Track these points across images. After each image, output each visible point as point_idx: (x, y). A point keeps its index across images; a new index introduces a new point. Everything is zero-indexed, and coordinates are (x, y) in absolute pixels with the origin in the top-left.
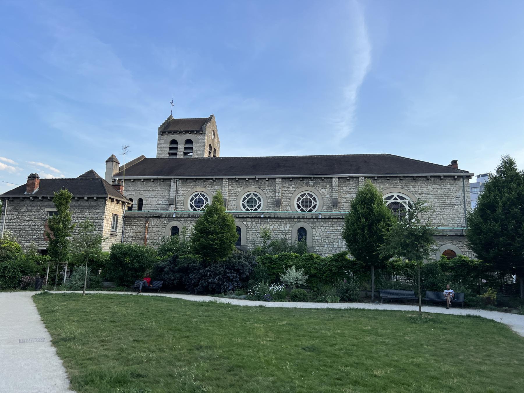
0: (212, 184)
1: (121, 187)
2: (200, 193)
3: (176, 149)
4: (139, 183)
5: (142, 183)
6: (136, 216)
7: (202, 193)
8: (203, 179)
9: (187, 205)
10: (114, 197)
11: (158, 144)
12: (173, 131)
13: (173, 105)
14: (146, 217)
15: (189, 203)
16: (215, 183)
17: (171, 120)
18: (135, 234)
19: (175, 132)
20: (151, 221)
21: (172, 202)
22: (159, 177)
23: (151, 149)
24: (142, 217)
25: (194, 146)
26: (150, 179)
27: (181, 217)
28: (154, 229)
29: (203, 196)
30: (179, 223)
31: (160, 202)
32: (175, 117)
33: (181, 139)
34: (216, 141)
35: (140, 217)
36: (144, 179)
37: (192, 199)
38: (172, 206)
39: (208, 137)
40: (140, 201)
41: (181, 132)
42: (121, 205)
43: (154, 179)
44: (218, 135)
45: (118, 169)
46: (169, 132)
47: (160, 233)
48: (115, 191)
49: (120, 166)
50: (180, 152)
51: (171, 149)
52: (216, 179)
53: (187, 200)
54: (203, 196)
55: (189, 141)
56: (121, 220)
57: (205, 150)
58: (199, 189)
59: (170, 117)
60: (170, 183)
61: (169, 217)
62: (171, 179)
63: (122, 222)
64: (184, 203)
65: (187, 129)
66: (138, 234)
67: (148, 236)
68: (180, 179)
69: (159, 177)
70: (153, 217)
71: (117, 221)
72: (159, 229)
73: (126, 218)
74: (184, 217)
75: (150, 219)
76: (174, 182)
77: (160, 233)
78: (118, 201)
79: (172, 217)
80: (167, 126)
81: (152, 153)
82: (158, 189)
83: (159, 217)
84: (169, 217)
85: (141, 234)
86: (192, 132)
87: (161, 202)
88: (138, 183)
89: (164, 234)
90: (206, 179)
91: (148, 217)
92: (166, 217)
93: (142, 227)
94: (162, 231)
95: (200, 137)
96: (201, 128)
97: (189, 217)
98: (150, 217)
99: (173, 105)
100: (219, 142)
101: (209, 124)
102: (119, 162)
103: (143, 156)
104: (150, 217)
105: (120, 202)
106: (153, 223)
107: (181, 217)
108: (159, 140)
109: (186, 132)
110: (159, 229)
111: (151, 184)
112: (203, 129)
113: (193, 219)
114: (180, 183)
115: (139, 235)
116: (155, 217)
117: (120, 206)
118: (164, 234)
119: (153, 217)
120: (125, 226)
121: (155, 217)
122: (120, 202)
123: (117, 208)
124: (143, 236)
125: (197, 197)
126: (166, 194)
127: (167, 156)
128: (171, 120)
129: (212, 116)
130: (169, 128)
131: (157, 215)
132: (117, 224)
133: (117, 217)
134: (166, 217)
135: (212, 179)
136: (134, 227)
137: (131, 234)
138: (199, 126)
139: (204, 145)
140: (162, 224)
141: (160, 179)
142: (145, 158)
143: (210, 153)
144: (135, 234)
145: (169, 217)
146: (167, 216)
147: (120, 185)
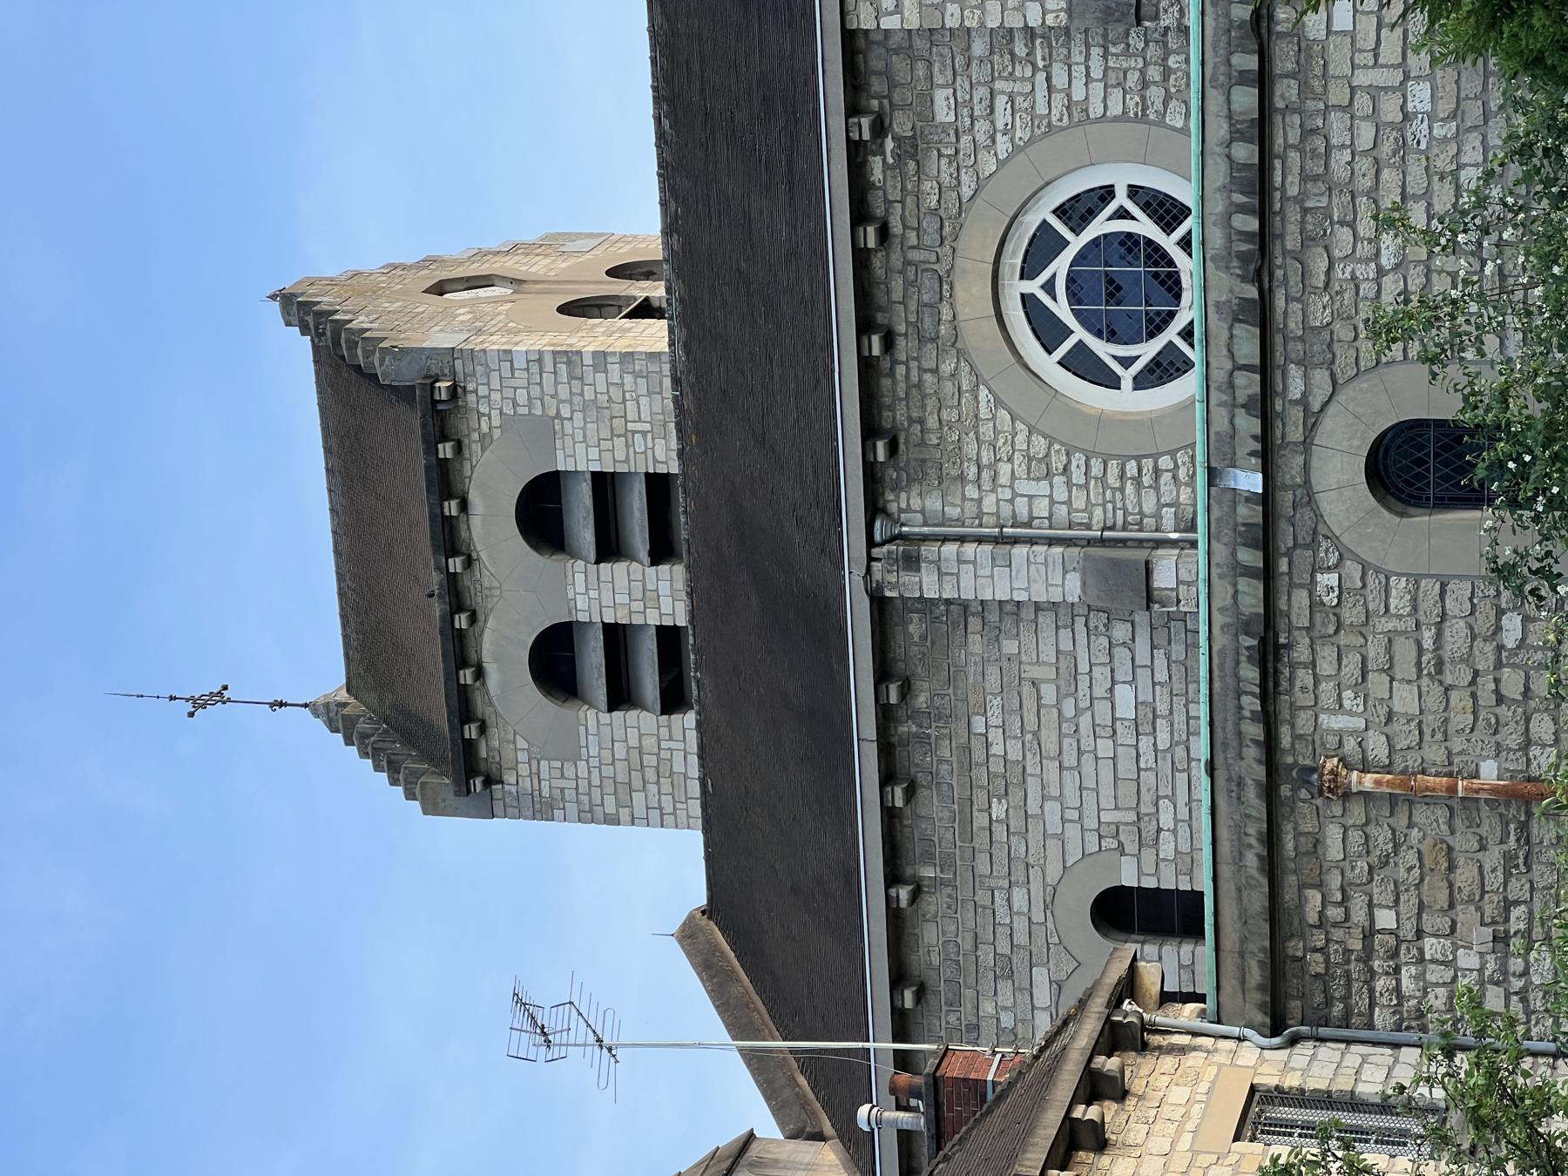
0: (912, 149)
1: (953, 1069)
2: (1015, 288)
3: (617, 637)
4: (930, 935)
5: (933, 903)
6: (1258, 900)
7: (1014, 259)
8: (861, 259)
9: (1152, 422)
10: (1051, 1121)
11: (587, 815)
12: (452, 677)
13: (220, 697)
14: (1270, 791)
15: (1127, 400)
16: (902, 124)
17: (355, 707)
18: (1466, 915)
19: (460, 651)
20: (1312, 741)
21: (1122, 578)
22: (864, 723)
23: (614, 876)
24: (1271, 839)
25: (581, 455)
26: (890, 816)
27: (1265, 406)
28: (1405, 700)
29: (1043, 247)
30: (1332, 423)
31: (1126, 709)
32: (327, 673)
33: (522, 596)
34: (537, 267)
35: (1272, 865)
36: (893, 878)
37: (1083, 365)
38: (1164, 578)
39: (504, 335)
40: (1119, 911)
41: (456, 596)
42: (1146, 1063)
43: (888, 777)
44: (482, 254)
45: (805, 1151)
46: (464, 707)
47: (1456, 634)
48: (995, 1121)
49: (767, 1127)
50: (650, 597)
51: (621, 696)
52: (853, 110)
53: (1102, 421)
54: (1043, 247)
55: (541, 512)
56: (1316, 1066)
57: (621, 345)
58: (971, 295)
59: (334, 717)
60: (926, 606)
61: (1265, 537)
62: (879, 604)
63: (1329, 1052)
64: (1136, 449)
65: (423, 538)
66: (1465, 876)
67: (1489, 772)
68: (874, 508)
69: (864, 723)
70: (1269, 719)
71: (1325, 1100)
72: (1405, 652)
73: (1286, 1004)
74: (1265, 368)
75: (1292, 753)
76: (911, 562)
77: (1456, 634)
78: (1095, 1087)
79: (1267, 499)
80: (408, 738)
81: (668, 866)
82: (994, 731)
83: (1269, 653)
84: (1269, 537)
85: (1464, 842)
86: (445, 482)
87: (1124, 694)
88: (931, 939)
89: (1459, 592)
90: (860, 214)
91: (1274, 777)
92: (1268, 575)
93: (1382, 837)
94: (1429, 605)
95: (490, 406)
96: (404, 394)
97: (1262, 314)
98: (1270, 745)
99: (220, 697)
100: (550, 244)
101: (360, 322)
102: (728, 1136)
103: (688, 935)
104: (1270, 745)
105: (1111, 1064)
106: (1338, 715)
107: (1265, 406)
108: (543, 809)
109: (449, 538)
110: (1405, 652)
111: (934, 811)
112: (408, 375)
113: (1285, 269)
114: (915, 506)
115: (1481, 861)
116: (1269, 691)
117: (1148, 1074)
118: (1459, 592)
119: (1269, 719)
120: (1382, 1018)
121: (1269, 691)
122: (1111, 1064)
123: (1179, 1095)
124: (1489, 825)
125: (1062, 309)
126: (1039, 650)
127: (690, 718)
128: (355, 707)
129: (300, 310)
130: (426, 722)
131: (1250, 673)
132: (1354, 1104)
133: (1280, 1096)
134: (1268, 575)
135: (857, 154)
136: (1385, 919)
137: (1468, 960)
138: (392, 420)
139: (570, 357)
140: (1352, 614)
141: (886, 716)
142: (709, 911)
143: (645, 310)
144: (1466, 915)
145: (1269, 537)
146: (1251, 557)
147: (935, 1081)
